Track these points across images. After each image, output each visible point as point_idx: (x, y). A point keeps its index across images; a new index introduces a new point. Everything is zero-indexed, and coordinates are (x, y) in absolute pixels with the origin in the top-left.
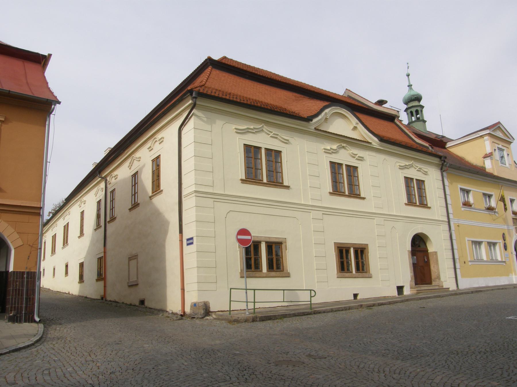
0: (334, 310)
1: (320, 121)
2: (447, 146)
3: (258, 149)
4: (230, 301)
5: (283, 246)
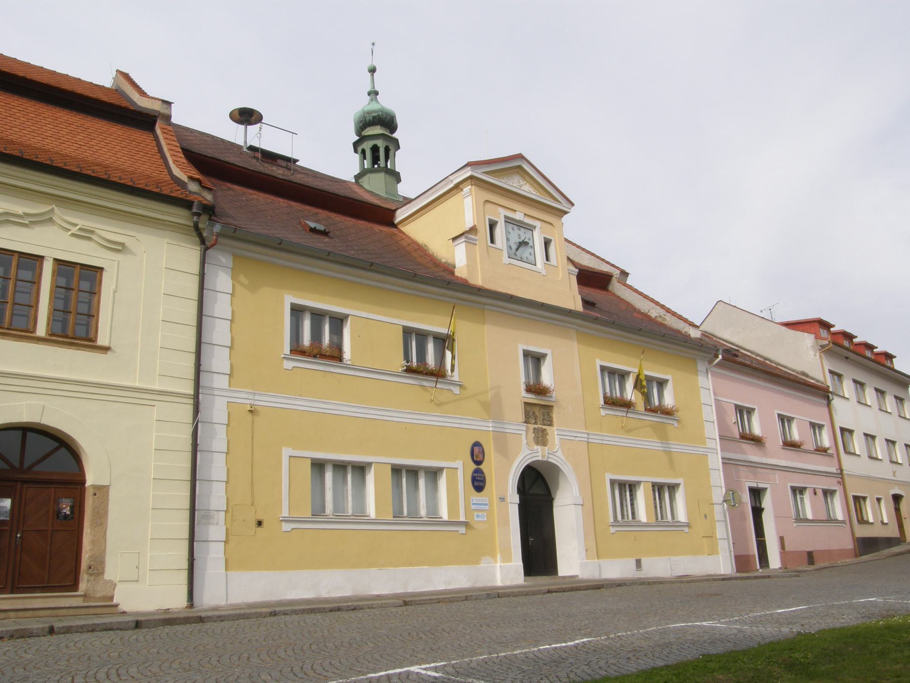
2: (397, 221)
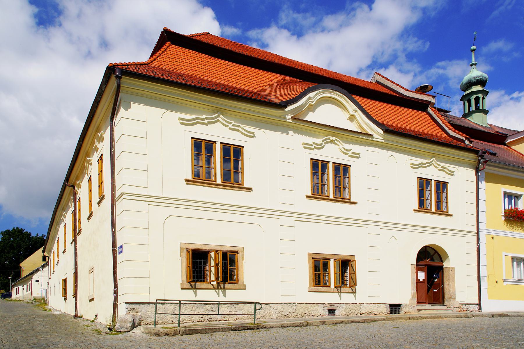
0: (285, 325)
1: (300, 109)
3: (210, 145)
4: (156, 314)
5: (240, 255)
